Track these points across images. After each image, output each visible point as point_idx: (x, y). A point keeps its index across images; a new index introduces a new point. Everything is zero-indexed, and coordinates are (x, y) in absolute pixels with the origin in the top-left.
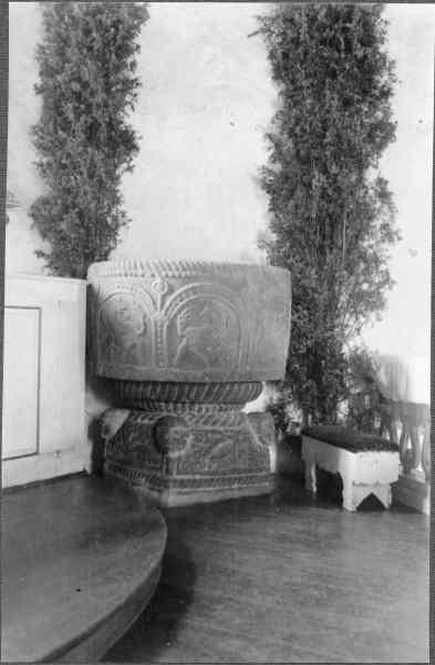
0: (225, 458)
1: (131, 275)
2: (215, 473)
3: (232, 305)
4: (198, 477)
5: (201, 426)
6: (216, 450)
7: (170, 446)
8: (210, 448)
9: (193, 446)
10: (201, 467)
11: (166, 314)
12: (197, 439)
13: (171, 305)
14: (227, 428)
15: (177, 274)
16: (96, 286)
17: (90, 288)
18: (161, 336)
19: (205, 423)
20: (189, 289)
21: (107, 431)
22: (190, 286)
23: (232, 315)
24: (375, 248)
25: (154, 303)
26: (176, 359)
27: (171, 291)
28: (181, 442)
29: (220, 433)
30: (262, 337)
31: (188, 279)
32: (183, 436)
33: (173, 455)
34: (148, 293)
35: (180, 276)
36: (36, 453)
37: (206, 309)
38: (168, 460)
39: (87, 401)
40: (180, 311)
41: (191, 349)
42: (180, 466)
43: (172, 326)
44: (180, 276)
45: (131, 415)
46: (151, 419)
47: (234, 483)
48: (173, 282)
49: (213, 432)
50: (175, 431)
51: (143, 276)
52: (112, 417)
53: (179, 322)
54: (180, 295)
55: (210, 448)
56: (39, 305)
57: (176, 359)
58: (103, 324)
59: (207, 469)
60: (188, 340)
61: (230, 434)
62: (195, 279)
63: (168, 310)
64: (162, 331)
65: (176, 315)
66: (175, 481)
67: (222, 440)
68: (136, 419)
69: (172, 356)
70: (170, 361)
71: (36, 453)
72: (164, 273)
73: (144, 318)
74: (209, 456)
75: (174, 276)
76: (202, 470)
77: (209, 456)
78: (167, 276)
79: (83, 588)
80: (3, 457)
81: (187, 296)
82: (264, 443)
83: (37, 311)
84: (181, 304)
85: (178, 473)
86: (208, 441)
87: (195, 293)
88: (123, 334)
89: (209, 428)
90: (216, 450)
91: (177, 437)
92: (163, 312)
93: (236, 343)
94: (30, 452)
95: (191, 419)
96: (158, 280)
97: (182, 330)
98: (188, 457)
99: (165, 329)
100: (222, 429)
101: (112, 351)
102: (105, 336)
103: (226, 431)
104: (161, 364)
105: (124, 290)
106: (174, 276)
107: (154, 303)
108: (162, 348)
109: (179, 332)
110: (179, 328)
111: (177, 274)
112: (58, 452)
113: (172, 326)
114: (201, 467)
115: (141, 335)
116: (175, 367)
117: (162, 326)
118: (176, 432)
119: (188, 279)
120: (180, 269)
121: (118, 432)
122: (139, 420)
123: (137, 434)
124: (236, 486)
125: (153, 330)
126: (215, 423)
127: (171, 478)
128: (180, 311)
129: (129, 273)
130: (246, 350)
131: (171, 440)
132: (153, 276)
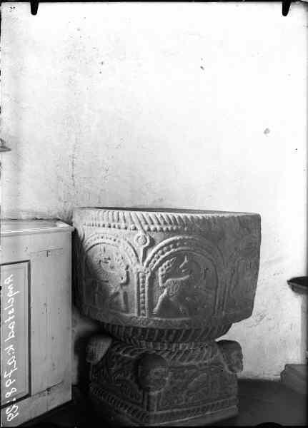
0: (200, 391)
1: (114, 227)
2: (192, 404)
3: (210, 256)
4: (175, 410)
5: (178, 363)
6: (191, 385)
7: (152, 387)
9: (171, 383)
10: (178, 402)
11: (147, 266)
12: (175, 376)
13: (153, 257)
14: (201, 362)
16: (80, 232)
17: (75, 234)
18: (143, 286)
19: (182, 360)
21: (93, 356)
22: (171, 239)
23: (212, 268)
25: (137, 256)
26: (156, 309)
27: (153, 243)
28: (160, 382)
29: (194, 367)
30: (237, 282)
32: (162, 376)
33: (154, 393)
34: (130, 244)
36: (28, 395)
37: (186, 261)
38: (149, 397)
39: (74, 322)
40: (161, 264)
41: (171, 299)
43: (153, 277)
45: (112, 346)
46: (132, 354)
47: (207, 410)
48: (154, 235)
49: (189, 367)
50: (157, 370)
51: (126, 228)
52: (96, 345)
53: (160, 273)
54: (162, 248)
56: (28, 259)
57: (156, 309)
58: (86, 265)
59: (183, 403)
60: (169, 290)
61: (204, 367)
63: (149, 262)
64: (144, 282)
66: (156, 416)
67: (196, 375)
68: (118, 350)
69: (152, 305)
71: (28, 395)
72: (146, 228)
73: (127, 267)
74: (186, 391)
75: (155, 230)
76: (180, 405)
77: (186, 391)
78: (149, 230)
79: (54, 341)
80: (2, 404)
81: (169, 250)
82: (232, 371)
83: (26, 264)
84: (162, 257)
85: (159, 409)
86: (183, 377)
87: (175, 247)
88: (107, 282)
89: (185, 364)
91: (157, 377)
92: (145, 264)
93: (214, 292)
94: (25, 394)
95: (168, 357)
96: (140, 233)
97: (164, 282)
98: (167, 393)
100: (197, 363)
101: (97, 295)
102: (90, 280)
103: (200, 365)
104: (142, 312)
105: (107, 241)
106: (155, 230)
107: (137, 256)
108: (144, 308)
109: (160, 285)
111: (158, 228)
112: (48, 389)
113: (153, 277)
114: (178, 402)
115: (122, 285)
116: (156, 316)
117: (144, 277)
118: (157, 373)
119: (172, 233)
120: (162, 222)
121: (102, 359)
122: (121, 353)
123: (120, 366)
124: (208, 413)
125: (136, 280)
126: (189, 360)
127: (152, 413)
128: (161, 264)
129: (112, 225)
131: (152, 381)
132: (135, 229)
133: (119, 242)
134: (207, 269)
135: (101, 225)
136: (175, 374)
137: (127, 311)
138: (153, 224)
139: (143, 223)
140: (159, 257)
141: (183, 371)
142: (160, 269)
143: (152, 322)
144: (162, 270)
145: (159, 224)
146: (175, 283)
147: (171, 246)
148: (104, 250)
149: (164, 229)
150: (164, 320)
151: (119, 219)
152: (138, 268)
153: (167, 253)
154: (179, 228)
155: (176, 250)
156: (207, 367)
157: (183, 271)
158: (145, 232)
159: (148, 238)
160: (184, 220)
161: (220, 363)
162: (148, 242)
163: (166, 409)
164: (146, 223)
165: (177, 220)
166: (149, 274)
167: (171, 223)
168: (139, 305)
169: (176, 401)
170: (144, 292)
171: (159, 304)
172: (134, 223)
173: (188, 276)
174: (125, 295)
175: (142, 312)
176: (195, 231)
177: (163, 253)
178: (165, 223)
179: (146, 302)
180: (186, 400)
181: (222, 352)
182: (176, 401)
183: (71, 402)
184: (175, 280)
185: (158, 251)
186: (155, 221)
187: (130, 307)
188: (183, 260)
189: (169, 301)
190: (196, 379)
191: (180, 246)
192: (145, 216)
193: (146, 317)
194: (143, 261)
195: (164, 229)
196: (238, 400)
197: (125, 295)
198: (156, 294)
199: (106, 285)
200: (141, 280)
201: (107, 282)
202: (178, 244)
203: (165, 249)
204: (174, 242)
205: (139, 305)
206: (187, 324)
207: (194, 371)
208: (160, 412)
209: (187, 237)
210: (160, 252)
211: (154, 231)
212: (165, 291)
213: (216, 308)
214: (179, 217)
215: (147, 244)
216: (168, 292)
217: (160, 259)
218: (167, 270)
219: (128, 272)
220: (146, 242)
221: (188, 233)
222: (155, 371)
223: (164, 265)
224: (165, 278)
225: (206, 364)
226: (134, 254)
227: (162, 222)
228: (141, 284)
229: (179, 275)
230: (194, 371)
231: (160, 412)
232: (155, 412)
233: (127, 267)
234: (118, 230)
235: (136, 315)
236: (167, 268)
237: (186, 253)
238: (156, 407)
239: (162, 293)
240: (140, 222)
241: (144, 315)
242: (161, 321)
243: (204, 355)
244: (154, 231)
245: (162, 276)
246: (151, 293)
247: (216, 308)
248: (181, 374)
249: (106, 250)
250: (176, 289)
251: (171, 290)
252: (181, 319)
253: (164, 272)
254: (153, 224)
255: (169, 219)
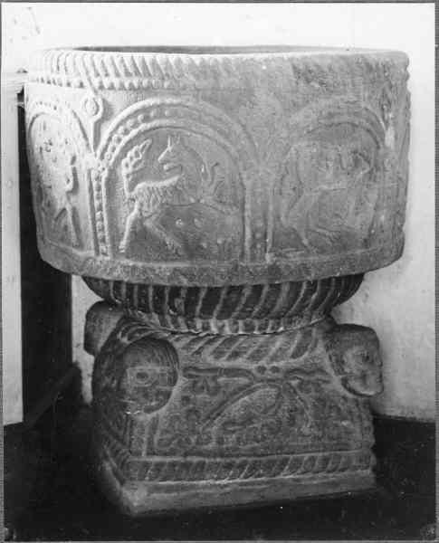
5: (208, 358)
6: (236, 409)
8: (223, 403)
9: (186, 399)
11: (102, 157)
13: (110, 139)
14: (263, 363)
15: (116, 82)
18: (99, 198)
19: (218, 354)
20: (137, 112)
24: (205, 194)
26: (123, 244)
29: (246, 373)
31: (139, 91)
35: (122, 87)
37: (169, 148)
41: (148, 224)
42: (156, 438)
43: (112, 182)
44: (122, 87)
48: (111, 97)
53: (124, 171)
54: (123, 122)
55: (223, 403)
60: (142, 205)
61: (269, 374)
62: (149, 91)
63: (105, 149)
65: (118, 160)
67: (247, 389)
69: (116, 238)
70: (115, 248)
72: (96, 82)
73: (74, 159)
75: (112, 87)
78: (101, 87)
81: (135, 125)
85: (151, 453)
89: (223, 363)
90: (236, 409)
91: (141, 383)
92: (99, 152)
95: (187, 347)
96: (89, 94)
97: (131, 188)
99: (103, 183)
100: (253, 366)
103: (262, 369)
106: (112, 87)
110: (125, 183)
111: (116, 82)
113: (112, 182)
117: (98, 178)
118: (141, 376)
119: (139, 91)
120: (122, 72)
126: (236, 355)
130: (260, 224)
131: (130, 391)
132: (81, 85)
133: (61, 110)
134: (217, 164)
135: (64, 82)
136: (195, 382)
137: (80, 246)
138: (107, 75)
139: (92, 74)
140: (119, 140)
141: (214, 379)
142: (124, 162)
143: (119, 269)
144: (127, 165)
145: (118, 75)
146: (151, 191)
147: (140, 117)
148: (45, 128)
149: (127, 85)
150: (140, 264)
151: (58, 68)
152: (91, 162)
153: (134, 132)
154: (153, 82)
155: (149, 125)
156: (280, 376)
157: (166, 167)
158: (96, 92)
159: (100, 103)
160: (162, 67)
161: (321, 370)
162: (101, 109)
163: (165, 454)
164: (98, 75)
165: (150, 68)
166: (106, 171)
167: (137, 73)
168: (95, 233)
169: (193, 439)
170: (100, 209)
171: (126, 234)
172: (79, 74)
173: (176, 178)
174: (74, 211)
175: (102, 247)
176: (184, 89)
177: (126, 132)
178: (128, 74)
179: (106, 229)
180: (220, 441)
181: (328, 348)
182: (193, 439)
183: (18, 425)
184: (152, 184)
185: (117, 127)
186: (111, 70)
187: (84, 239)
188: (165, 146)
189: (145, 229)
190: (246, 398)
191: (155, 117)
192: (137, 62)
193: (108, 258)
194: (96, 146)
195: (127, 85)
196: (373, 459)
197: (74, 211)
198: (123, 210)
199: (48, 193)
200: (95, 184)
201: (50, 187)
202: (152, 114)
203: (129, 123)
204: (145, 110)
205: (95, 233)
206: (185, 275)
207: (243, 381)
208: (157, 459)
209: (168, 101)
210: (121, 129)
211: (109, 89)
212: (136, 206)
213: (247, 245)
214: (154, 63)
215: (99, 115)
216: (140, 210)
217: (122, 144)
218: (134, 166)
219: (74, 170)
220: (98, 110)
221: (174, 91)
222: (138, 369)
223: (129, 154)
224: (136, 178)
225: (276, 370)
226: (82, 135)
227: (122, 72)
228: (95, 193)
229: (159, 176)
230: (243, 381)
231: (157, 459)
232: (144, 458)
233: (74, 159)
234: (67, 89)
235: (92, 253)
236: (135, 160)
237: (173, 132)
238: (145, 447)
239: (132, 210)
240: (87, 73)
241: (105, 254)
242: (134, 268)
243: (273, 349)
244: (109, 89)
245: (128, 176)
246: (112, 213)
247: (247, 245)
248: (212, 384)
249: (47, 125)
250: (154, 203)
251: (145, 204)
252: (172, 265)
253: (130, 169)
254: (107, 75)
255: (134, 65)
